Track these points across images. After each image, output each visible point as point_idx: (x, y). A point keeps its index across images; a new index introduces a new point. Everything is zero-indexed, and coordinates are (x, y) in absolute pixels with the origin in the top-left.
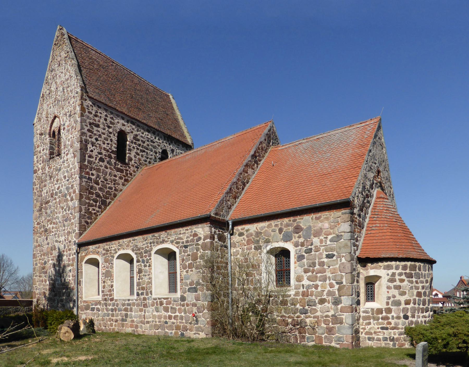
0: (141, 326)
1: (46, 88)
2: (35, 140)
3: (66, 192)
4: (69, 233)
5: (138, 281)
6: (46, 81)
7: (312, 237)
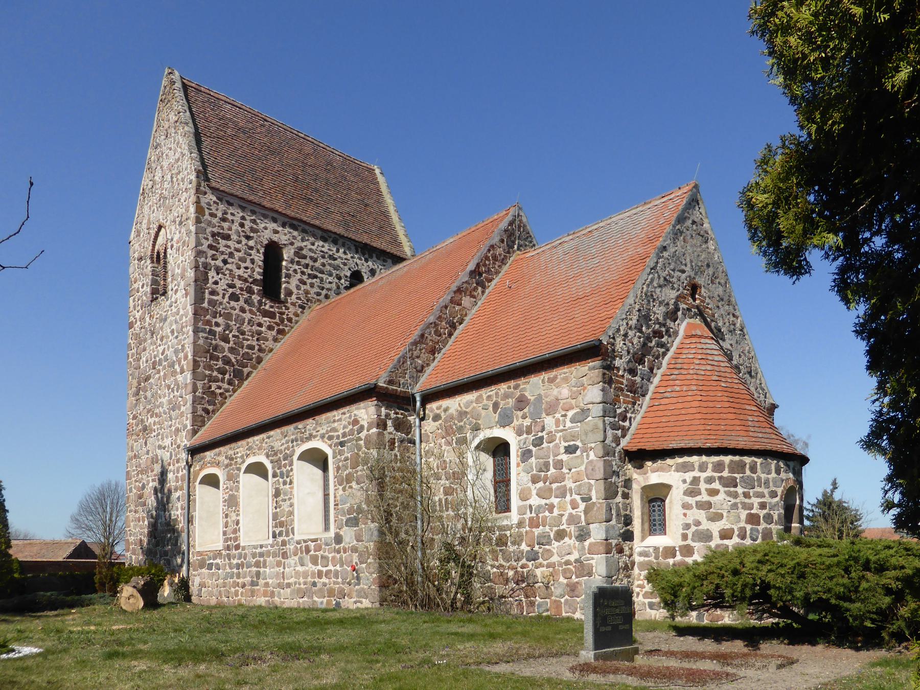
0: (279, 593)
1: (148, 178)
2: (131, 270)
3: (174, 358)
4: (178, 430)
5: (274, 511)
6: (149, 166)
7: (544, 415)
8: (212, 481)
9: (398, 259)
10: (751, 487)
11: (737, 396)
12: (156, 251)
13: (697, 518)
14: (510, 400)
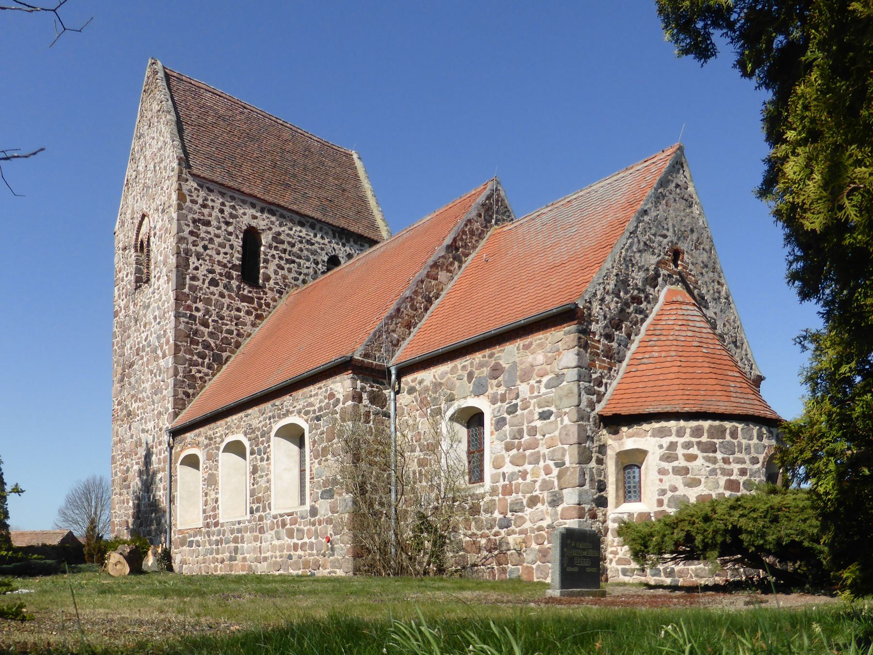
2: (116, 260)
3: (157, 344)
5: (252, 487)
7: (518, 382)
8: (192, 462)
9: (373, 242)
10: (730, 452)
11: (719, 362)
12: (140, 240)
13: (673, 484)
14: (485, 369)
